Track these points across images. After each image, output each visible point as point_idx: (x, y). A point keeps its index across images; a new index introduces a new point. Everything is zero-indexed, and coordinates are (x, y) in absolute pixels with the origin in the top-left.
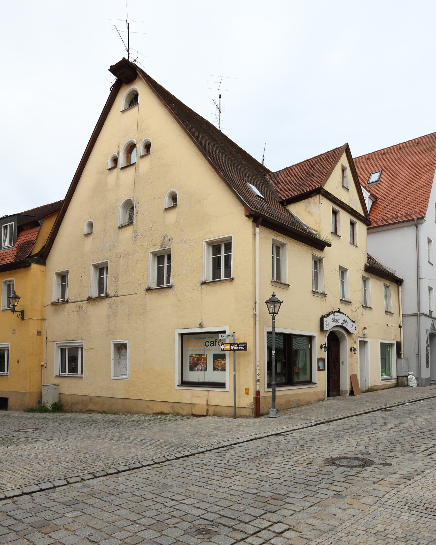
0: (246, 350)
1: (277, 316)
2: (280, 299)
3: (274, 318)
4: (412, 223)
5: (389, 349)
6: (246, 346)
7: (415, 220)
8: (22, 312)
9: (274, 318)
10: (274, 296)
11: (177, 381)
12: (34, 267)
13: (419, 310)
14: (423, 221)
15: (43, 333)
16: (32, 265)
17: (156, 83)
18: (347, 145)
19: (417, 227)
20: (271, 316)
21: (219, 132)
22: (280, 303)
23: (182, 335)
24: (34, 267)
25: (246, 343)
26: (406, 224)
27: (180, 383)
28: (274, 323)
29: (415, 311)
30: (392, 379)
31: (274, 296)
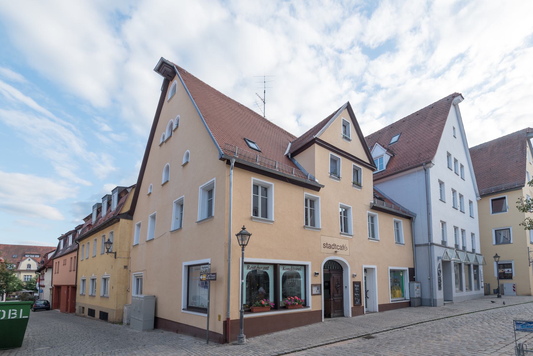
0: (215, 280)
1: (246, 248)
2: (249, 232)
3: (243, 250)
4: (422, 167)
5: (401, 275)
6: (216, 276)
7: (424, 164)
8: (115, 253)
9: (243, 250)
10: (244, 229)
11: (183, 304)
12: (122, 221)
13: (430, 240)
14: (432, 165)
15: (129, 267)
16: (121, 220)
17: (215, 90)
18: (348, 103)
19: (425, 170)
20: (240, 248)
21: (263, 120)
22: (250, 235)
23: (189, 267)
24: (122, 221)
25: (215, 274)
26: (416, 169)
27: (186, 307)
28: (243, 253)
29: (426, 242)
30: (405, 299)
31: (244, 229)
